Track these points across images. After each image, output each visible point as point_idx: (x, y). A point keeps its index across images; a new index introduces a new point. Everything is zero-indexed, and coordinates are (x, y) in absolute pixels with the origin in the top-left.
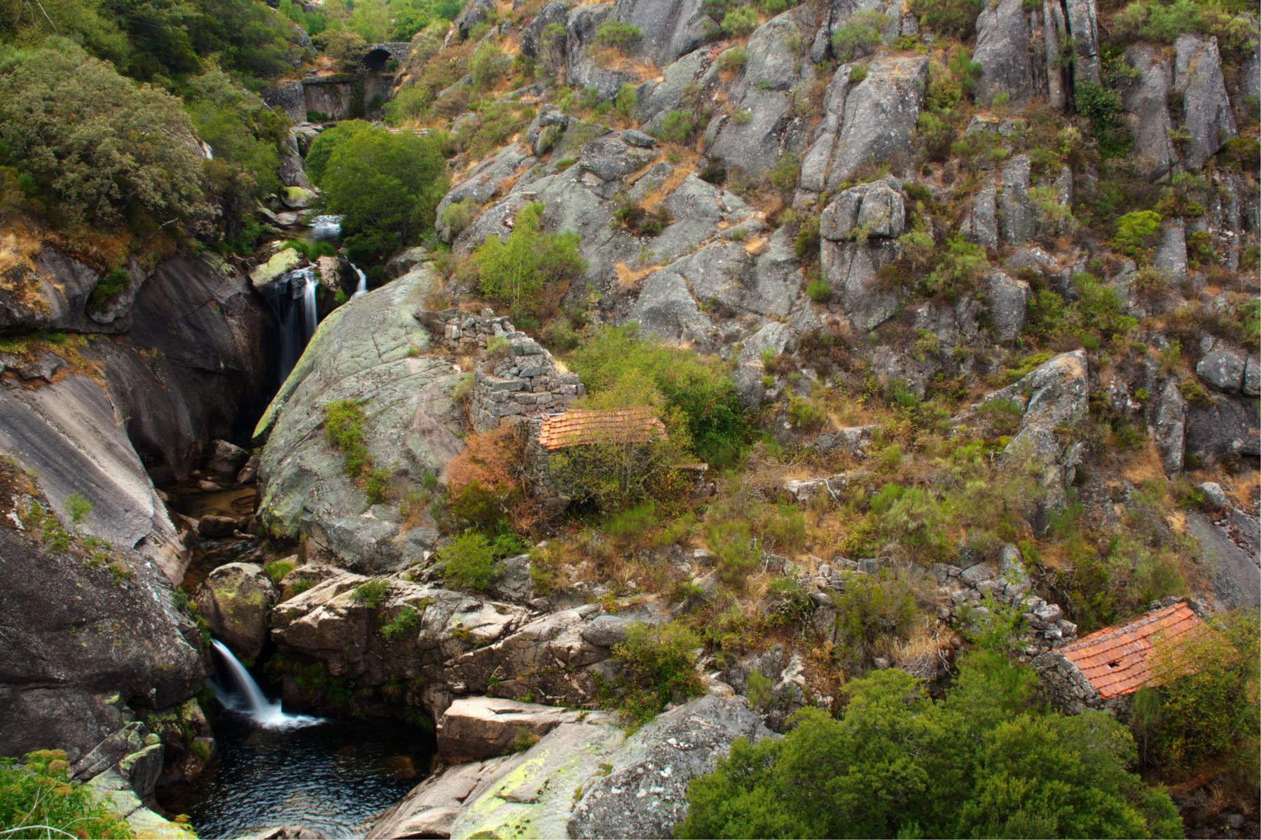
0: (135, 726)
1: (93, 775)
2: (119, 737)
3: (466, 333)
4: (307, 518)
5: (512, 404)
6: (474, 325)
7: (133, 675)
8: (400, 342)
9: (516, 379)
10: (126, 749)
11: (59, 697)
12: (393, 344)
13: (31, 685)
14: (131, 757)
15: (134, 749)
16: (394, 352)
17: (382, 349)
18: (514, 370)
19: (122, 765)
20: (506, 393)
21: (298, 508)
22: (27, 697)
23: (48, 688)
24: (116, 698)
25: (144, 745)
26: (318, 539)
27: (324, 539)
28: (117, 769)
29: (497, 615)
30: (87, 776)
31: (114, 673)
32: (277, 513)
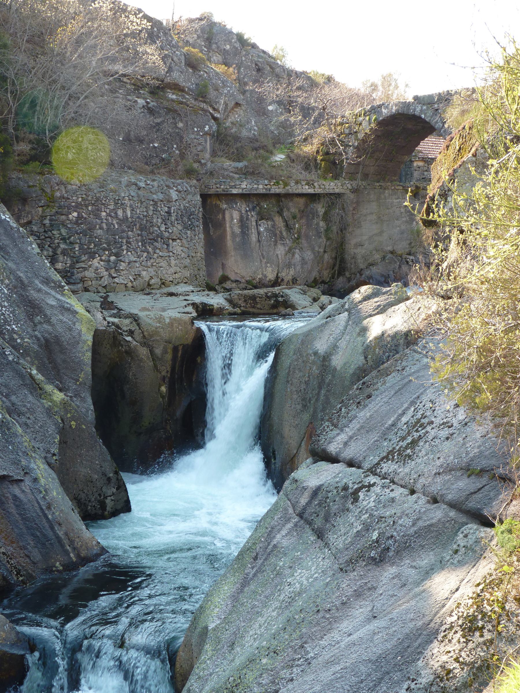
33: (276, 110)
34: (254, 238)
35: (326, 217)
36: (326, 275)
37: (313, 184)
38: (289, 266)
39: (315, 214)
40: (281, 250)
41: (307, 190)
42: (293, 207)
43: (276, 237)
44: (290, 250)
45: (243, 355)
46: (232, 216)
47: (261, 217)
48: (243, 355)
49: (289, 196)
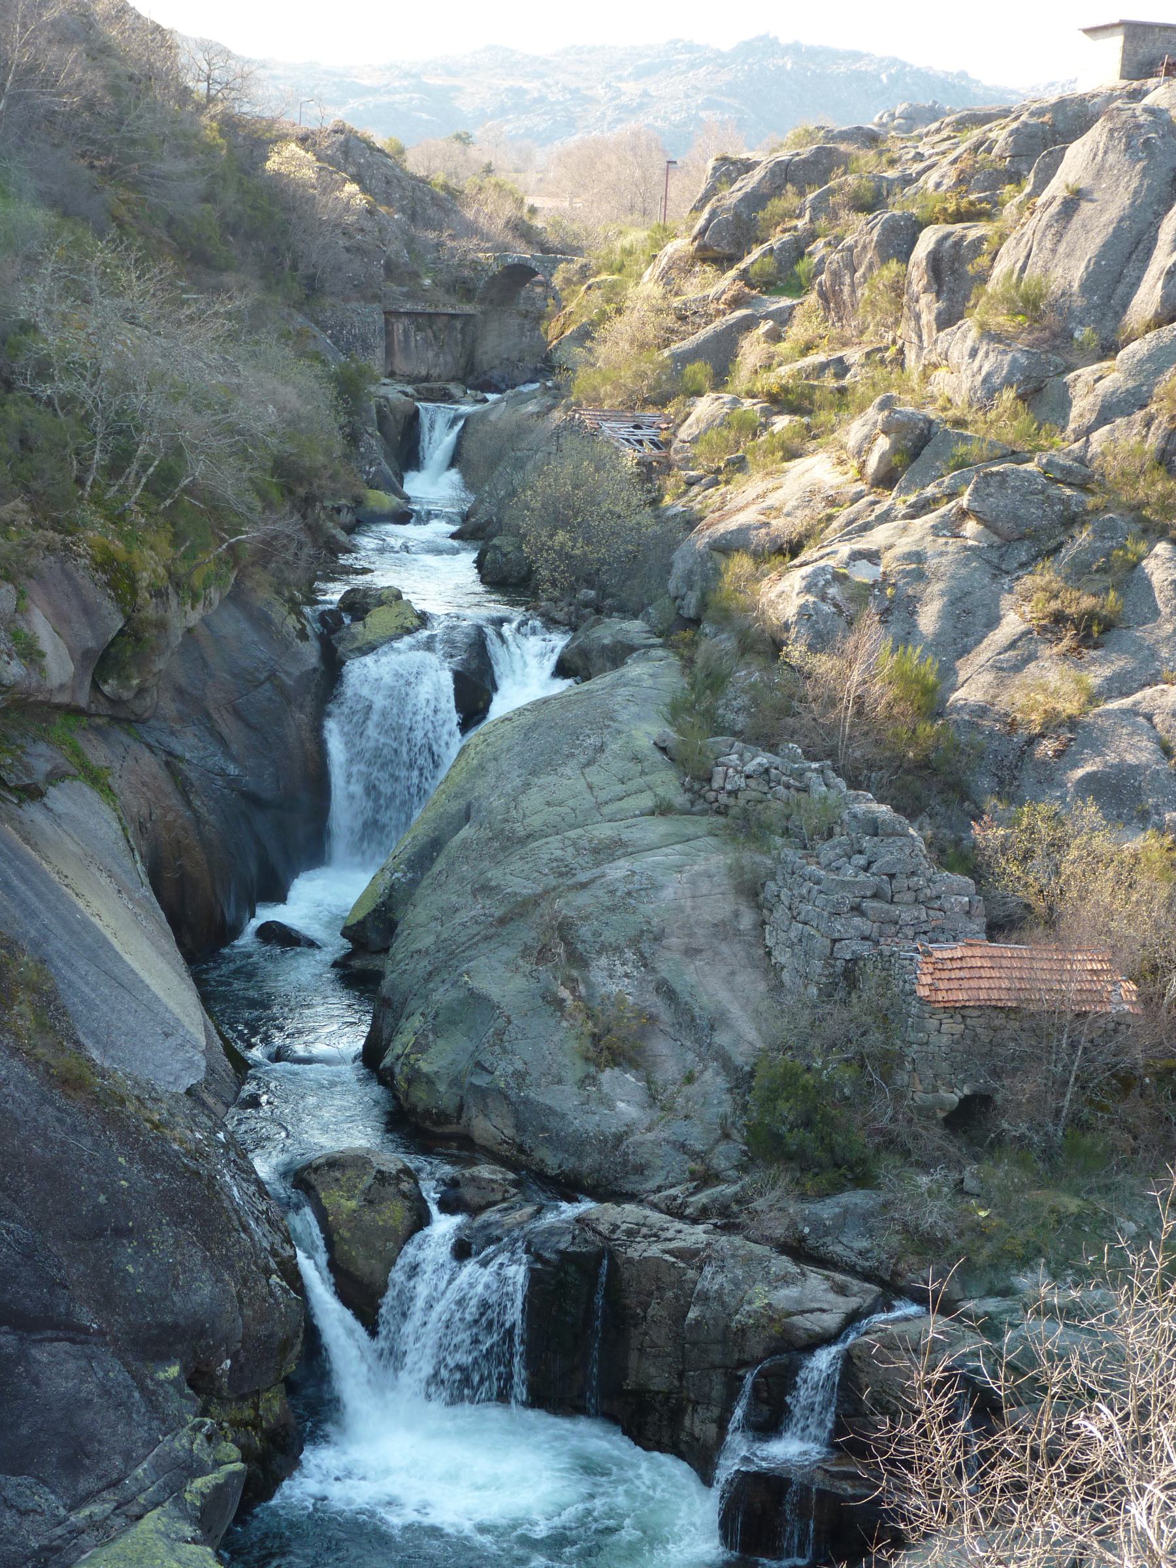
0: (202, 1425)
1: (146, 1510)
2: (180, 1443)
3: (752, 783)
4: (481, 1081)
5: (857, 921)
6: (767, 771)
7: (202, 1333)
8: (632, 785)
9: (862, 876)
10: (194, 1468)
11: (89, 1358)
12: (619, 789)
13: (49, 1333)
14: (199, 1483)
15: (202, 1471)
16: (623, 804)
17: (603, 796)
18: (861, 860)
19: (188, 1496)
20: (850, 899)
21: (465, 1064)
22: (41, 1354)
23: (73, 1341)
24: (174, 1371)
25: (218, 1464)
26: (498, 1122)
27: (510, 1121)
28: (179, 1501)
29: (831, 1296)
30: (135, 1510)
31: (176, 1326)
32: (425, 1067)
34: (413, 344)
35: (463, 331)
36: (460, 374)
38: (436, 366)
39: (454, 328)
40: (430, 354)
41: (451, 311)
42: (440, 323)
43: (427, 344)
44: (437, 355)
45: (441, 422)
46: (399, 328)
47: (418, 329)
48: (441, 422)
49: (437, 314)
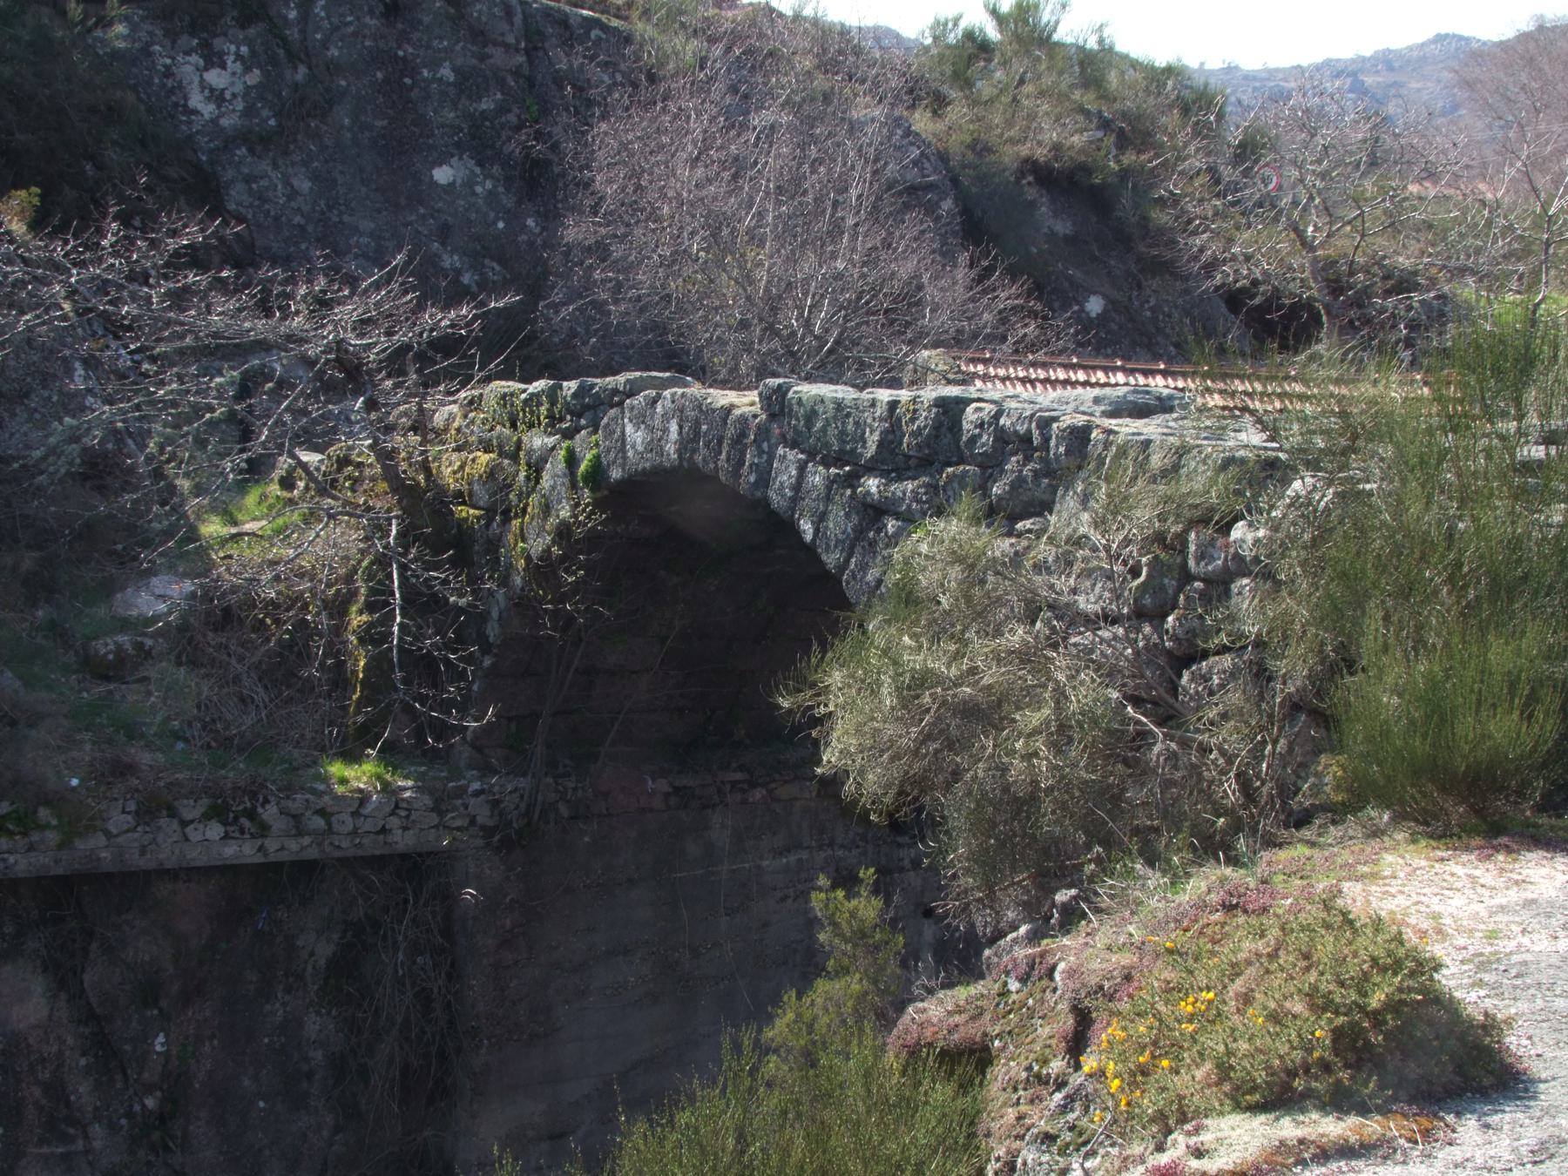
33: (469, 183)
37: (252, 815)
